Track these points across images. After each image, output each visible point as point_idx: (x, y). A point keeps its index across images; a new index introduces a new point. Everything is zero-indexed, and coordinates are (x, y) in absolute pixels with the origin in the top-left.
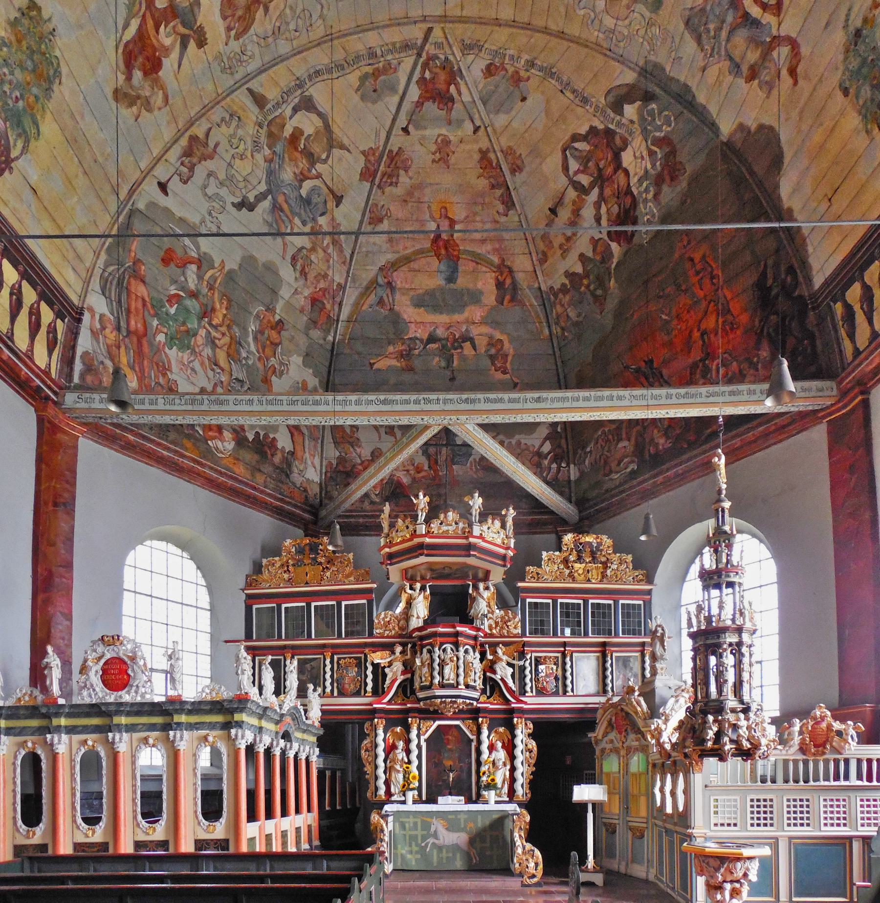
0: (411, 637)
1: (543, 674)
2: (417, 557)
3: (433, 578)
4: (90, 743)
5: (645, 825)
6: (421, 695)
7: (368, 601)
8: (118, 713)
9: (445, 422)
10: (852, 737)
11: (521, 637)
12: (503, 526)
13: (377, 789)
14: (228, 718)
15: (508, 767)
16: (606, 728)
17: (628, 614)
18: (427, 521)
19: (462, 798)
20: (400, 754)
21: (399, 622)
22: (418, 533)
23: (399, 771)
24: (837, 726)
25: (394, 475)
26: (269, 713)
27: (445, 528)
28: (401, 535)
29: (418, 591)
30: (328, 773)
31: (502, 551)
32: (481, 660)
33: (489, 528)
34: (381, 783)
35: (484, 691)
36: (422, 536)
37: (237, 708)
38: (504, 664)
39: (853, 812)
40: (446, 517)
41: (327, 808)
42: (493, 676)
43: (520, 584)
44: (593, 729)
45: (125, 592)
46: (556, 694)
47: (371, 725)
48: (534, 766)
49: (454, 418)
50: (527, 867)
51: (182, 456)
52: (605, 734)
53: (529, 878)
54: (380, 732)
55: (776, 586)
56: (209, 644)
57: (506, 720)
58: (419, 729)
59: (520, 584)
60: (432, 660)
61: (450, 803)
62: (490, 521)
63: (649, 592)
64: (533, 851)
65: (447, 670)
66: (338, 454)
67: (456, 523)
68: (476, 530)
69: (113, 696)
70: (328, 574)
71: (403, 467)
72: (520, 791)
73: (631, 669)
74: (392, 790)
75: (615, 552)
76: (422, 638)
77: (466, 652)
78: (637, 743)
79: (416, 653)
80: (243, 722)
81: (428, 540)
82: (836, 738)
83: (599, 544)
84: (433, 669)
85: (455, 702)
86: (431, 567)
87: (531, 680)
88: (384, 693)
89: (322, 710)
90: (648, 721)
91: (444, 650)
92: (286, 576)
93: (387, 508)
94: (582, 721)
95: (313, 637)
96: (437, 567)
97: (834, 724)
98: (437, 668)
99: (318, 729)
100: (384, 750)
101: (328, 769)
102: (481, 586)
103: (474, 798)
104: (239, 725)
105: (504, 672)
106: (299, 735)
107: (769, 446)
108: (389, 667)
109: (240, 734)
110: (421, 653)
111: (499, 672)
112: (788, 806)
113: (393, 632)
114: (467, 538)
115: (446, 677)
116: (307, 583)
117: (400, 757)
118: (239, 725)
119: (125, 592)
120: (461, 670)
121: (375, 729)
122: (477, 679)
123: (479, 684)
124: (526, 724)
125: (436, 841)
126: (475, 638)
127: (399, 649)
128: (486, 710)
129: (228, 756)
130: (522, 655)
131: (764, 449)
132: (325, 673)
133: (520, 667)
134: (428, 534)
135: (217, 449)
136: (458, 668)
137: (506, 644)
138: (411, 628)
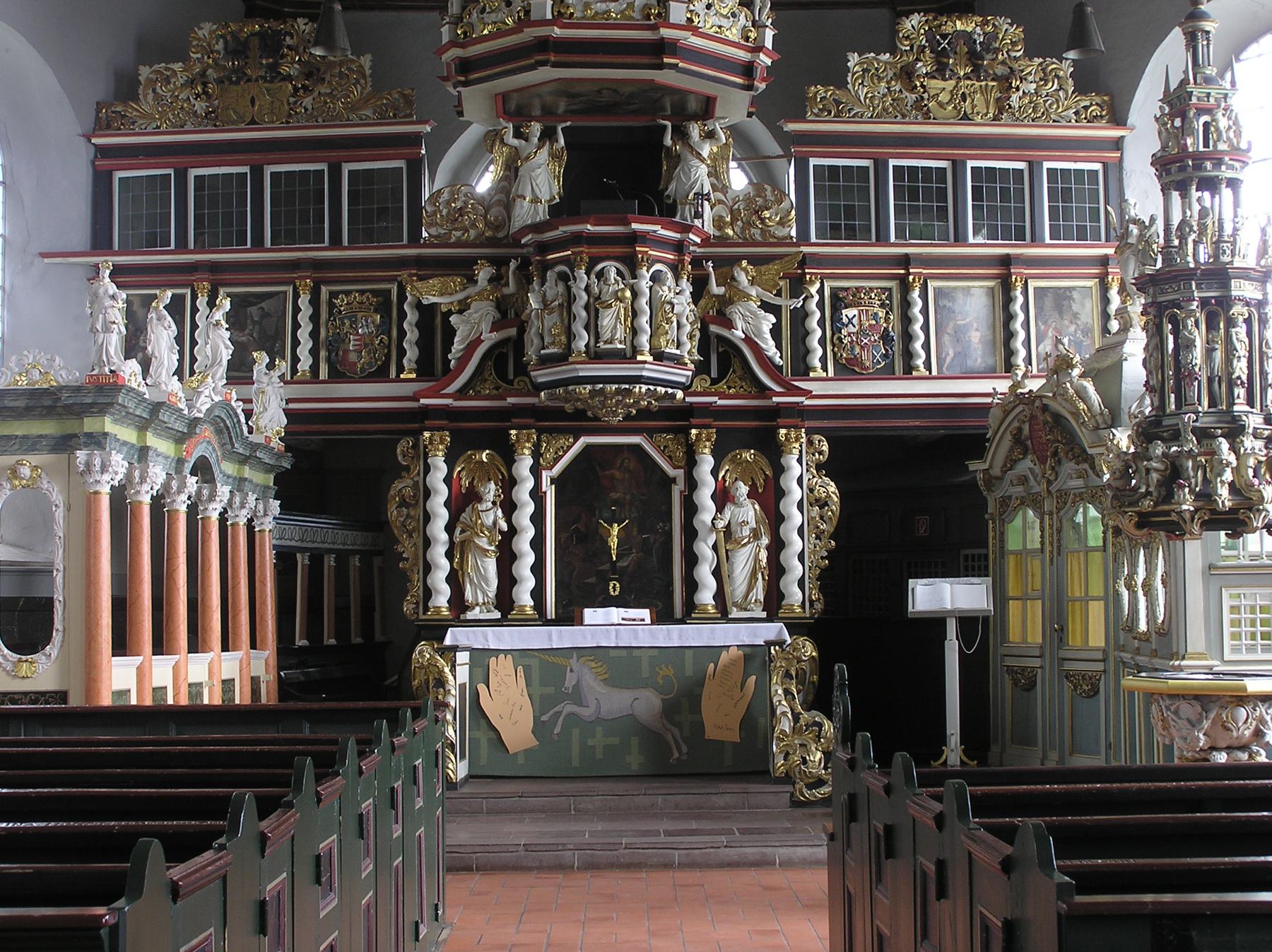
0: (516, 243)
3: (573, 112)
5: (1100, 666)
6: (542, 376)
13: (428, 593)
15: (765, 541)
20: (491, 515)
21: (487, 212)
22: (534, 16)
29: (536, 140)
31: (743, 55)
34: (439, 579)
35: (702, 368)
36: (544, 23)
38: (754, 305)
42: (725, 333)
46: (887, 373)
47: (415, 446)
48: (833, 536)
50: (804, 761)
58: (536, 455)
60: (570, 299)
64: (820, 725)
65: (606, 320)
72: (794, 595)
76: (544, 248)
77: (656, 278)
79: (530, 281)
81: (557, 32)
84: (571, 317)
85: (628, 392)
86: (566, 89)
88: (449, 373)
91: (601, 275)
96: (578, 89)
98: (584, 314)
100: (447, 504)
102: (695, 130)
108: (460, 312)
111: (740, 324)
113: (473, 233)
114: (655, 28)
115: (606, 335)
117: (489, 520)
120: (644, 320)
122: (684, 339)
126: (679, 247)
127: (484, 274)
128: (707, 410)
132: (296, 326)
136: (635, 314)
137: (755, 260)
138: (517, 224)
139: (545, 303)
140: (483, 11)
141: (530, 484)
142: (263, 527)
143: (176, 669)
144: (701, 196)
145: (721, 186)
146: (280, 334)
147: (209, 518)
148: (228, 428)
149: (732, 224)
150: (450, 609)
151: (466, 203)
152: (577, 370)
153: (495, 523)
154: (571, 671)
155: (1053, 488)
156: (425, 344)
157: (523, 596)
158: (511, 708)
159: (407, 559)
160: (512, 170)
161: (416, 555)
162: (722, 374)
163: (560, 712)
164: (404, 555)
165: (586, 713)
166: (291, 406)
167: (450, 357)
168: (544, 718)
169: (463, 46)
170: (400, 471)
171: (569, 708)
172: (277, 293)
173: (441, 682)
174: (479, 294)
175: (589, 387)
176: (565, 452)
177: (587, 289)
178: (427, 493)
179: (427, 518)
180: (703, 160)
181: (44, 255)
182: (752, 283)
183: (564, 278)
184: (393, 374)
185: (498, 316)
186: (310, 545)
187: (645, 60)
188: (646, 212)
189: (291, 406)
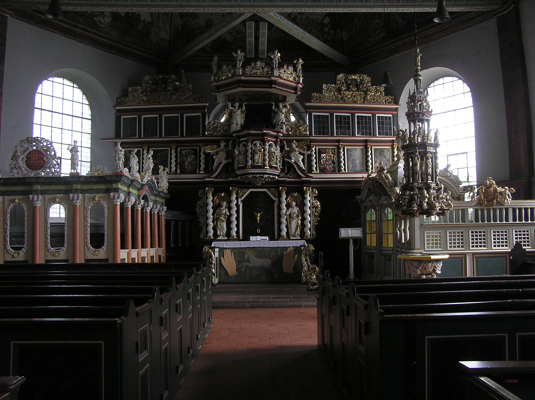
0: (232, 136)
1: (324, 160)
2: (236, 88)
4: (17, 201)
5: (392, 252)
6: (239, 172)
7: (202, 114)
8: (37, 183)
9: (255, 11)
10: (508, 195)
11: (309, 137)
12: (295, 70)
13: (207, 232)
14: (109, 186)
15: (300, 218)
16: (367, 193)
17: (383, 123)
18: (244, 67)
19: (267, 238)
21: (224, 127)
22: (237, 74)
24: (499, 189)
25: (204, 265)
26: (134, 183)
27: (255, 71)
28: (226, 76)
30: (172, 223)
31: (294, 85)
32: (281, 151)
33: (285, 71)
35: (283, 170)
37: (115, 180)
38: (297, 153)
39: (511, 238)
40: (255, 65)
41: (172, 246)
42: (289, 161)
43: (307, 104)
44: (359, 194)
45: (35, 110)
46: (334, 172)
47: (204, 192)
49: (260, 9)
50: (311, 278)
51: (77, 27)
52: (367, 197)
53: (312, 285)
55: (472, 108)
56: (90, 141)
57: (297, 189)
58: (237, 194)
59: (307, 104)
60: (247, 151)
61: (258, 241)
62: (285, 67)
63: (396, 110)
64: (315, 268)
65: (256, 157)
66: (183, 22)
67: (262, 68)
68: (276, 73)
69: (33, 173)
70: (174, 97)
71: (229, 32)
73: (385, 156)
75: (372, 85)
76: (239, 137)
77: (270, 146)
78: (386, 202)
80: (119, 188)
82: (499, 196)
83: (362, 80)
84: (247, 156)
85: (263, 177)
87: (316, 163)
88: (213, 172)
90: (393, 188)
91: (255, 145)
92: (145, 98)
93: (216, 59)
94: (351, 189)
95: (163, 136)
97: (498, 188)
99: (166, 194)
100: (212, 208)
102: (281, 105)
103: (276, 238)
104: (117, 190)
105: (297, 159)
106: (153, 198)
107: (464, 28)
108: (216, 155)
109: (116, 196)
110: (239, 146)
112: (472, 236)
114: (270, 77)
116: (159, 103)
118: (117, 190)
119: (35, 110)
121: (206, 194)
123: (279, 165)
124: (312, 191)
125: (248, 264)
126: (276, 137)
127: (223, 144)
128: (284, 182)
129: (108, 209)
130: (309, 148)
131: (462, 29)
132: (171, 159)
133: (308, 155)
134: (244, 74)
135: (100, 22)
136: (264, 155)
138: (232, 131)
139: (240, 153)
140: (223, 72)
143: (138, 253)
144: (282, 123)
145: (288, 120)
149: (291, 131)
151: (218, 125)
155: (379, 203)
158: (230, 264)
160: (230, 116)
162: (288, 172)
169: (217, 82)
170: (199, 199)
171: (246, 264)
174: (222, 150)
177: (251, 149)
180: (283, 113)
182: (296, 147)
183: (245, 146)
187: (267, 86)
188: (268, 128)
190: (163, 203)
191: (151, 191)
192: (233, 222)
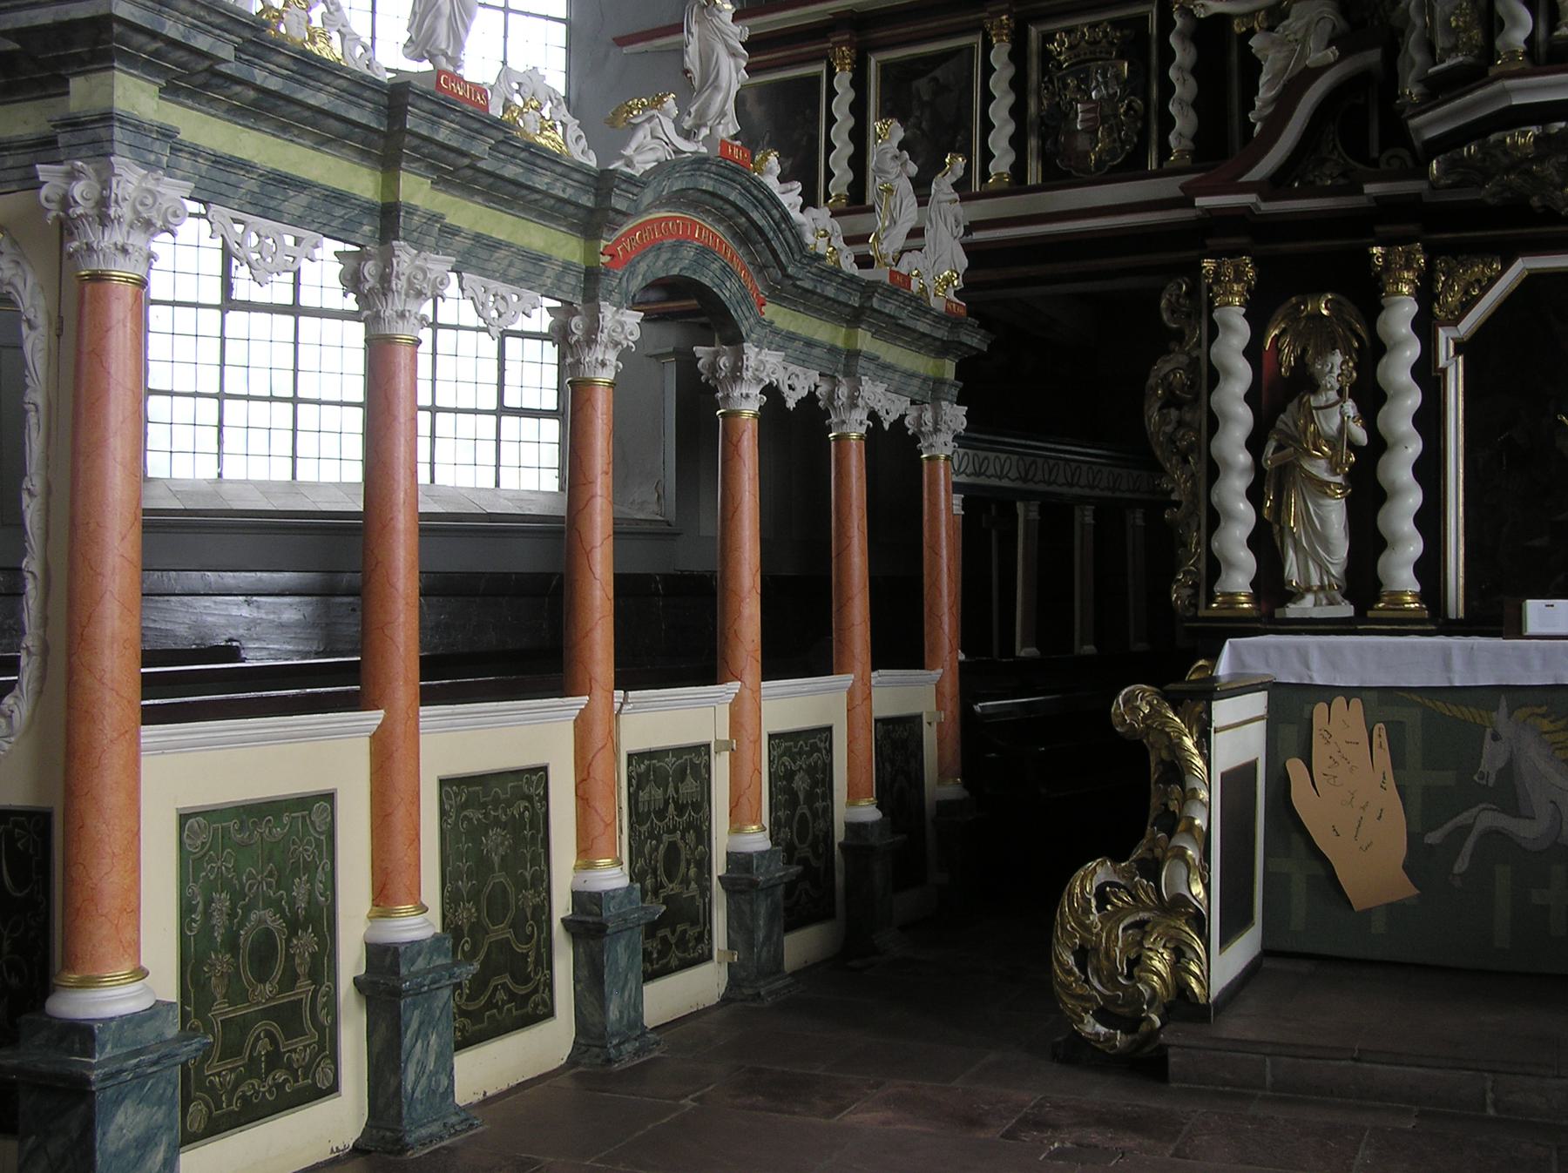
6: (1430, 125)
13: (1215, 567)
20: (1337, 416)
23: (1322, 487)
34: (1235, 540)
47: (1193, 292)
54: (1236, 330)
58: (1425, 295)
74: (1292, 569)
89: (969, 249)
100: (1251, 398)
101: (1027, 496)
117: (1331, 424)
132: (988, 98)
141: (1412, 351)
142: (935, 452)
143: (583, 726)
146: (961, 122)
147: (737, 413)
148: (760, 230)
150: (1255, 597)
152: (1506, 93)
153: (1342, 428)
154: (1496, 737)
156: (1210, 105)
157: (1401, 573)
158: (1360, 817)
159: (1178, 504)
161: (1194, 494)
163: (1468, 829)
164: (1174, 497)
165: (1527, 831)
166: (978, 236)
167: (1252, 117)
168: (1433, 838)
170: (1163, 340)
171: (1487, 818)
172: (957, 51)
173: (1177, 770)
175: (1533, 131)
176: (1484, 291)
178: (1214, 377)
179: (1213, 424)
181: (622, 41)
184: (1152, 164)
185: (1342, 25)
186: (1042, 487)
189: (978, 236)
190: (939, 382)
191: (761, 269)
192: (1397, 492)
